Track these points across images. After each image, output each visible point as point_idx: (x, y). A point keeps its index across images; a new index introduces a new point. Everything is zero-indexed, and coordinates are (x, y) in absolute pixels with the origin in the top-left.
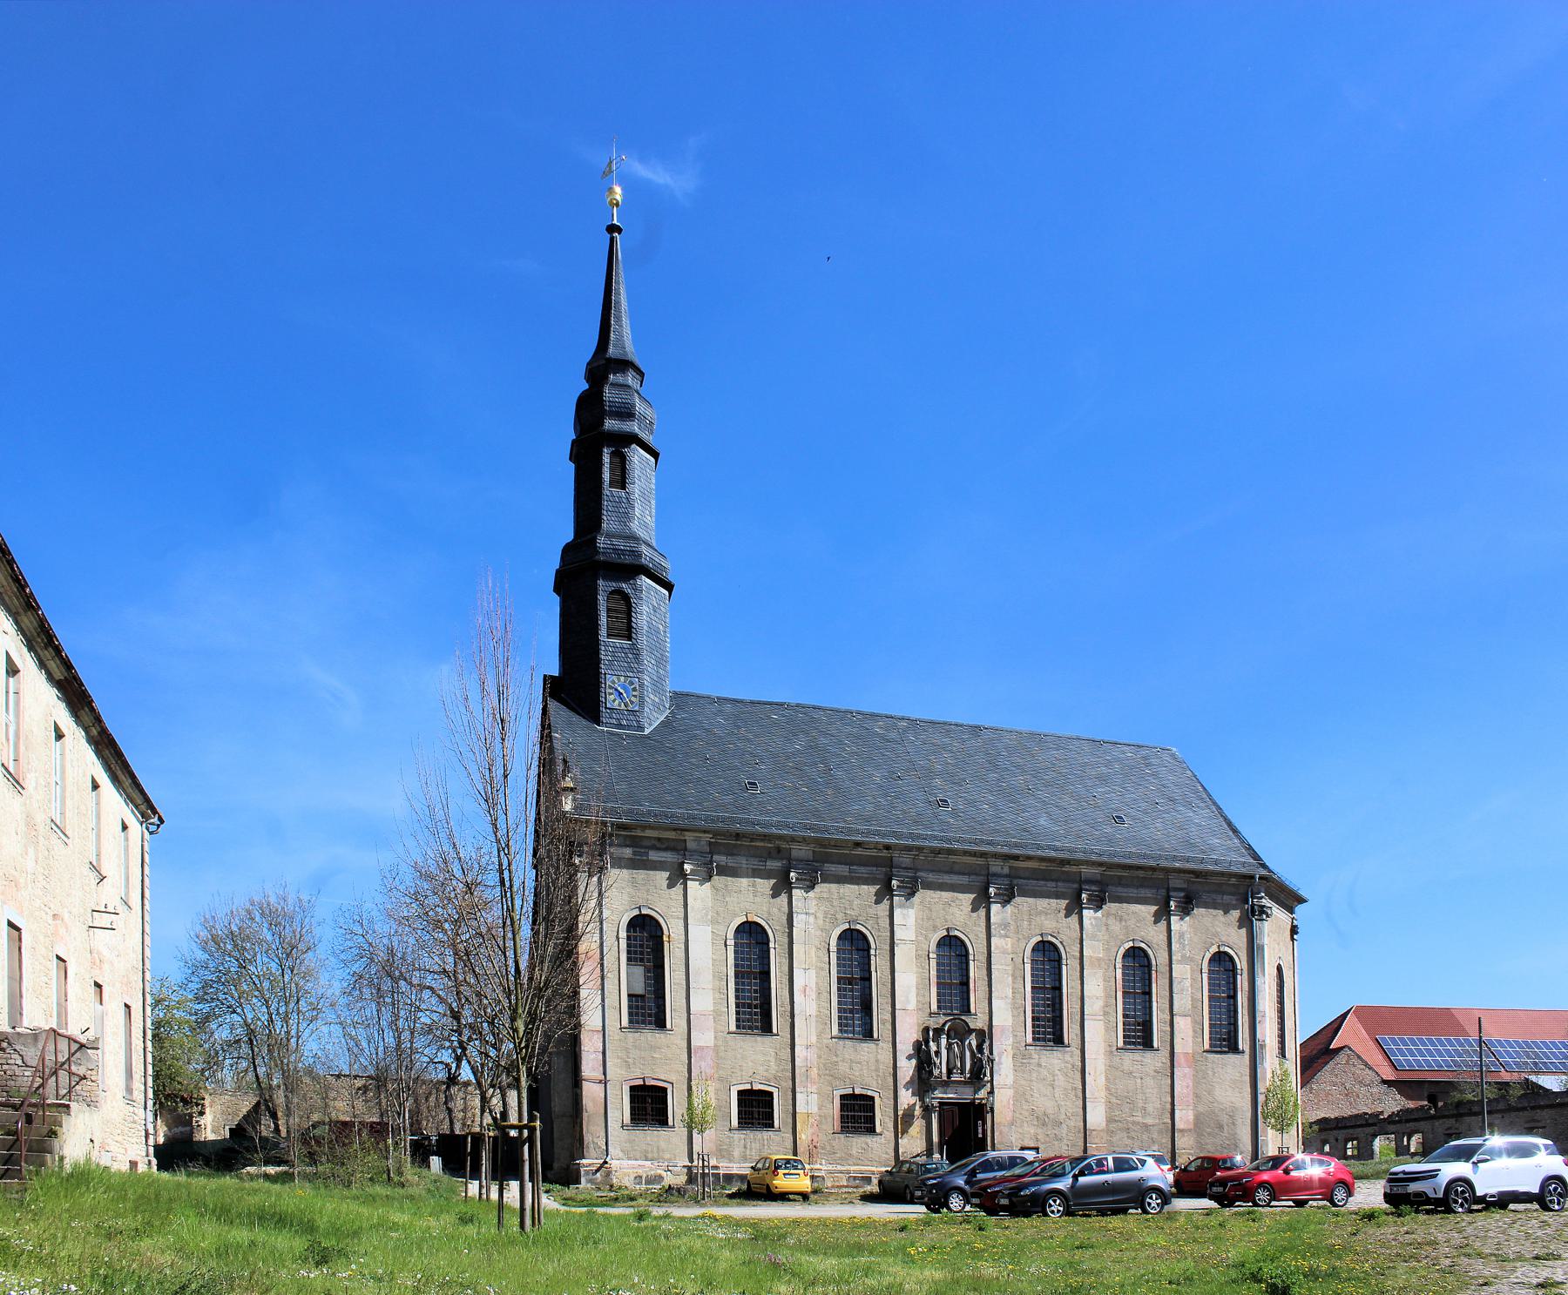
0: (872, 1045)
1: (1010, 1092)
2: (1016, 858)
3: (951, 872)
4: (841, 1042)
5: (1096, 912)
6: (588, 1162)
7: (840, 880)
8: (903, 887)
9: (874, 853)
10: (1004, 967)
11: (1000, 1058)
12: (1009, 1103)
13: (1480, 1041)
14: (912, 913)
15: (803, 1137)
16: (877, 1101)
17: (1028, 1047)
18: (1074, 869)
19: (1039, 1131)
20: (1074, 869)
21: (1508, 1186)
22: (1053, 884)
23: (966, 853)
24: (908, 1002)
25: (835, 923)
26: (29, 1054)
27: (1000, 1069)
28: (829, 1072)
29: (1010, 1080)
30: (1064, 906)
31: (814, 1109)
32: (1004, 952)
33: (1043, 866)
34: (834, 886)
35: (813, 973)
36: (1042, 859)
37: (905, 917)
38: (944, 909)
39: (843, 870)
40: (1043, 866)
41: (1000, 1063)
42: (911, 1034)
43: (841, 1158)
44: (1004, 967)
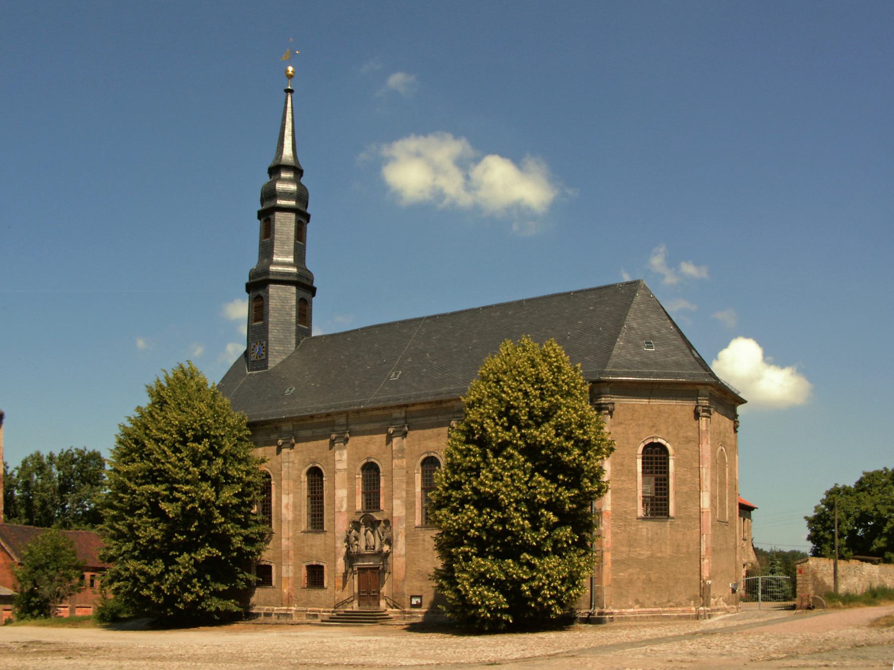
0: (323, 535)
1: (403, 560)
2: (407, 406)
3: (371, 422)
4: (306, 535)
5: (291, 449)
6: (99, 614)
7: (307, 439)
8: (397, 431)
9: (323, 420)
10: (401, 478)
11: (397, 537)
12: (402, 567)
13: (421, 527)
14: (345, 452)
15: (285, 591)
16: (325, 569)
17: (416, 529)
18: (449, 404)
19: (423, 584)
20: (449, 404)
21: (240, 658)
22: (436, 418)
23: (373, 409)
24: (342, 506)
25: (360, 459)
26: (874, 490)
27: (397, 544)
28: (298, 550)
29: (403, 552)
30: (328, 443)
31: (291, 575)
32: (401, 468)
33: (428, 407)
34: (304, 444)
35: (291, 496)
36: (423, 403)
37: (341, 455)
38: (365, 446)
39: (308, 433)
40: (428, 407)
41: (397, 541)
42: (343, 526)
43: (305, 603)
44: (401, 478)
